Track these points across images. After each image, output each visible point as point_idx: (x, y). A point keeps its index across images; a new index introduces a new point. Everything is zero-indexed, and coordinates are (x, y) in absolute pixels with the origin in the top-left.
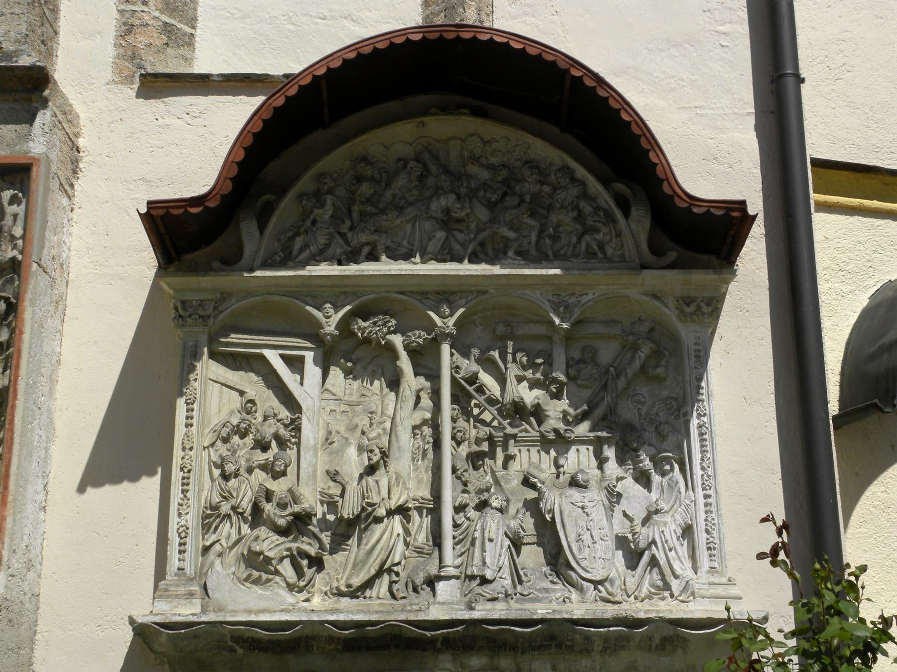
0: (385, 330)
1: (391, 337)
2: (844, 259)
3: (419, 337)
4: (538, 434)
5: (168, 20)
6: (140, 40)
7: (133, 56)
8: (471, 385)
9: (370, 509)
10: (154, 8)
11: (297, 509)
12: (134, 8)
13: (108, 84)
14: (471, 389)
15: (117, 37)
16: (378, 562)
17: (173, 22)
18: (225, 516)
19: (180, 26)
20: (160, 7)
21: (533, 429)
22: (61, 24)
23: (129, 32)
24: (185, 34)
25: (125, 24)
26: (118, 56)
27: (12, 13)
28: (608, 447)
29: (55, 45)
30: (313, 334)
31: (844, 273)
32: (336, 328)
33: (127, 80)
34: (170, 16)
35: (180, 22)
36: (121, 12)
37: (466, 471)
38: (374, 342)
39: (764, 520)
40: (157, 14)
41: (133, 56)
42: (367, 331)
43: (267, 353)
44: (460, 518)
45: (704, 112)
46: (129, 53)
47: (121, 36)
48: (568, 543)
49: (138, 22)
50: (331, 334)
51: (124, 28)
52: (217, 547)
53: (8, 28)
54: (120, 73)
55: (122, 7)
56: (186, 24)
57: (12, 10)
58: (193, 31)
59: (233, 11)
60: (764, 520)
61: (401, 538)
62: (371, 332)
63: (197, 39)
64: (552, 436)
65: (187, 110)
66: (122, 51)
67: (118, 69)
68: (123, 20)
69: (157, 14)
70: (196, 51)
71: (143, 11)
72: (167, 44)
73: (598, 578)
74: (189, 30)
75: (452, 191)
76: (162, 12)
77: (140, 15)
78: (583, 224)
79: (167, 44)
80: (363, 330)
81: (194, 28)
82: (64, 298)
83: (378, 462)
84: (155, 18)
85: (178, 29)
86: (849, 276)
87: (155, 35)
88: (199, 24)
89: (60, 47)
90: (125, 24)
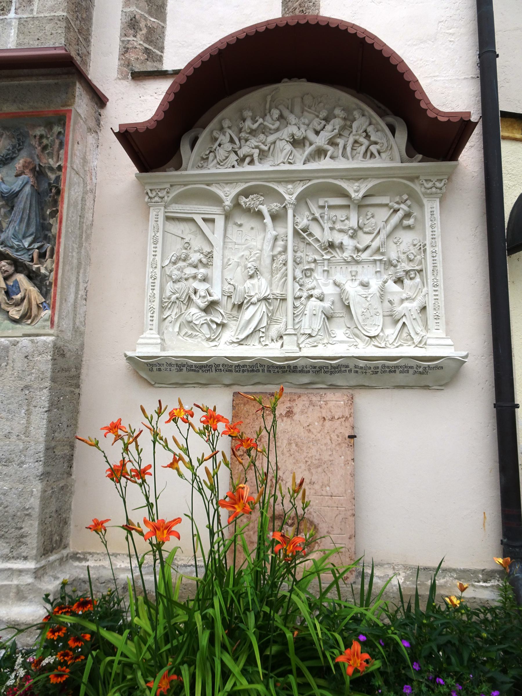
0: (258, 203)
1: (261, 207)
2: (511, 168)
3: (275, 206)
4: (342, 258)
5: (147, 46)
6: (132, 56)
7: (128, 64)
8: (304, 232)
9: (249, 298)
10: (140, 39)
11: (210, 299)
12: (129, 39)
13: (115, 80)
14: (305, 235)
15: (119, 56)
16: (254, 327)
17: (150, 47)
18: (173, 302)
19: (154, 50)
20: (143, 39)
21: (339, 256)
22: (92, 49)
23: (126, 52)
24: (157, 55)
25: (124, 48)
26: (121, 65)
27: (57, 33)
28: (470, 116)
29: (88, 60)
30: (217, 201)
31: (510, 175)
32: (231, 202)
33: (125, 78)
34: (149, 45)
35: (154, 48)
36: (123, 42)
37: (301, 279)
38: (252, 211)
39: (105, 436)
40: (142, 43)
41: (128, 64)
42: (248, 204)
43: (195, 217)
44: (297, 303)
45: (439, 79)
46: (127, 63)
47: (122, 54)
48: (357, 316)
49: (131, 46)
50: (229, 206)
51: (124, 50)
52: (169, 318)
53: (54, 41)
54: (121, 74)
55: (123, 39)
56: (158, 50)
57: (57, 31)
58: (162, 54)
59: (183, 43)
60: (105, 436)
61: (265, 314)
62: (250, 204)
63: (164, 58)
64: (349, 259)
65: (156, 91)
66: (123, 62)
67: (120, 72)
68: (124, 45)
69: (142, 43)
70: (164, 65)
71: (133, 40)
72: (147, 59)
73: (373, 335)
74: (159, 53)
75: (295, 124)
76: (144, 42)
77: (132, 42)
78: (369, 140)
79: (147, 59)
80: (246, 203)
81: (162, 52)
82: (94, 191)
83: (253, 273)
84: (140, 44)
85: (154, 52)
86: (513, 177)
87: (140, 54)
88: (166, 50)
89: (91, 62)
90: (124, 48)
